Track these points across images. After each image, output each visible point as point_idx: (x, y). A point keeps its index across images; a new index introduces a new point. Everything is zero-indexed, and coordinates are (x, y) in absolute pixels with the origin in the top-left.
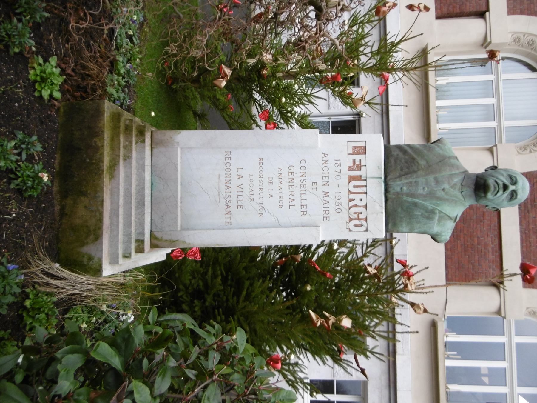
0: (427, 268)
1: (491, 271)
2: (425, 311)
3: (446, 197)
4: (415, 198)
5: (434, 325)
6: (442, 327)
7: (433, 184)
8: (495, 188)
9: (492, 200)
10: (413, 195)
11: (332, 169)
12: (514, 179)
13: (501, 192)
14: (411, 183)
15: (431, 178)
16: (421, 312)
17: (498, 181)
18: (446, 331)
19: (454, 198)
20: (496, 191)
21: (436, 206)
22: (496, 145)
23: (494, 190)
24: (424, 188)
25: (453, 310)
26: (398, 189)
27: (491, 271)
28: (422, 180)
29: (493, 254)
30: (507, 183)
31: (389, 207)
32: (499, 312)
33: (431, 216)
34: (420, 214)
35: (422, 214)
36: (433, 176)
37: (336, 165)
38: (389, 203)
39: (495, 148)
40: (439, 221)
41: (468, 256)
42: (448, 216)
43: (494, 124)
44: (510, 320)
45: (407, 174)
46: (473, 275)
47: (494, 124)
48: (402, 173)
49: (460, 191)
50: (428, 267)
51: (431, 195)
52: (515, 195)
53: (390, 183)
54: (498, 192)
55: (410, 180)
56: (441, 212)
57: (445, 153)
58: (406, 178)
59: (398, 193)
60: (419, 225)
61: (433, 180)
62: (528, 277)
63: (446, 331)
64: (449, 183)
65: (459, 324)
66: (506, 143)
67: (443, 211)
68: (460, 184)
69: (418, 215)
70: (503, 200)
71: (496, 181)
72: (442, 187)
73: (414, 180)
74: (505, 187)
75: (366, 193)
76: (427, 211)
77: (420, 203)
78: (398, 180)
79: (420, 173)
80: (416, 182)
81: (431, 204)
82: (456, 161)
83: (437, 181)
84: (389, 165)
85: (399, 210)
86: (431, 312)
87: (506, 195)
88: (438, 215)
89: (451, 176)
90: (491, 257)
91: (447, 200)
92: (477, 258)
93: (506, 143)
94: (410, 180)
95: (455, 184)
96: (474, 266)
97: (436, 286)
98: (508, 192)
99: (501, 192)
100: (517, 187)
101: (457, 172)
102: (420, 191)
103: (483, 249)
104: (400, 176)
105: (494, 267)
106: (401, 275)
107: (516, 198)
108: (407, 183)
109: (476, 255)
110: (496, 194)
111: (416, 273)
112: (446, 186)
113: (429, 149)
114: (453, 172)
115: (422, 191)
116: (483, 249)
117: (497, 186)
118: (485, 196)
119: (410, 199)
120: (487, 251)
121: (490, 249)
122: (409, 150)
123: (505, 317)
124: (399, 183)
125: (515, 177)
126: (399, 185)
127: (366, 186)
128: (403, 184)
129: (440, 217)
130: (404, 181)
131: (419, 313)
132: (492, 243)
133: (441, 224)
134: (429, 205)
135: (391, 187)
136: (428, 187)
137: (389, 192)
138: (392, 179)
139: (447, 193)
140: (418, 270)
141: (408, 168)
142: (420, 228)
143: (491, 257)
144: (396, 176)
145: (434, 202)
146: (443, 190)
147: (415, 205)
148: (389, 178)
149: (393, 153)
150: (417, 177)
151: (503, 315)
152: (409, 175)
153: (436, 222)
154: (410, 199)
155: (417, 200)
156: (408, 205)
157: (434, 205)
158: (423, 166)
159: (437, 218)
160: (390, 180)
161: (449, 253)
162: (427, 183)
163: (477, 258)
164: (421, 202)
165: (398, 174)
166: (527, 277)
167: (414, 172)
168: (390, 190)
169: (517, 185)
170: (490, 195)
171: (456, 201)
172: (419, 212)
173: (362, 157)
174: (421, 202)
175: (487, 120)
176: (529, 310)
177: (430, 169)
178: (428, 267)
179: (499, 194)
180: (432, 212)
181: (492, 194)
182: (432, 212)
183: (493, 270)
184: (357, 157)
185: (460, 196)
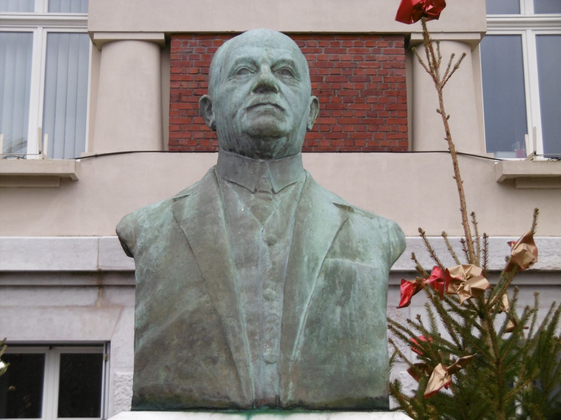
0: (423, 234)
1: (380, 57)
2: (528, 239)
3: (289, 236)
4: (297, 324)
5: (511, 183)
6: (513, 164)
7: (255, 272)
8: (266, 113)
9: (296, 117)
10: (289, 330)
12: (242, 65)
13: (277, 98)
14: (252, 334)
15: (238, 277)
16: (532, 248)
17: (248, 104)
18: (522, 154)
19: (293, 213)
20: (276, 110)
21: (316, 264)
22: (91, 34)
23: (273, 114)
24: (267, 298)
25: (471, 134)
26: (270, 371)
27: (380, 57)
28: (244, 304)
29: (343, 52)
30: (252, 82)
31: (321, 400)
32: (471, 45)
33: (343, 279)
34: (338, 310)
35: (339, 303)
36: (233, 270)
38: (309, 398)
39: (97, 37)
40: (354, 255)
41: (346, 102)
42: (341, 229)
43: (39, 36)
44: (489, 22)
45: (225, 345)
46: (391, 94)
47: (39, 36)
48: (223, 357)
49: (271, 196)
50: (420, 230)
51: (289, 277)
52: (283, 65)
53: (250, 397)
54: (276, 106)
55: (245, 337)
56: (331, 252)
57: (166, 229)
58: (238, 349)
59: (282, 374)
60: (369, 312)
61: (243, 270)
62: (431, 7)
63: (522, 154)
64: (252, 227)
65: (504, 130)
66: (87, 11)
67: (329, 244)
68: (253, 197)
69: (343, 315)
70: (295, 92)
71: (249, 109)
72: (265, 246)
73: (245, 325)
74: (265, 88)
76: (328, 290)
77: (310, 309)
78: (242, 373)
79: (223, 306)
80: (249, 321)
81: (310, 280)
82: (187, 202)
83: (248, 260)
84: (196, 395)
85: (330, 369)
86: (531, 226)
87: (283, 87)
88: (339, 260)
89: (234, 221)
90: (348, 56)
91: (298, 235)
92: (351, 85)
93: (87, 11)
94: (245, 337)
95: (254, 209)
96: (369, 92)
97: (463, 210)
98: (278, 82)
99: (277, 98)
100: (264, 61)
101: (219, 203)
102: (276, 308)
103: (330, 71)
104: (231, 363)
105: (370, 49)
106: (443, 298)
107: (292, 63)
108: (253, 346)
109: (344, 85)
110: (282, 110)
111: (436, 260)
112: (260, 236)
113: (154, 277)
114: (221, 214)
115: (275, 303)
116: (330, 71)
117: (261, 108)
118: (287, 135)
119: (300, 339)
120: (335, 63)
121: (331, 56)
122: (150, 335)
123: (483, 34)
124: (252, 369)
125: (237, 63)
126: (258, 369)
128: (256, 357)
129: (344, 254)
130: (247, 352)
131: (536, 253)
132: (317, 51)
133: (361, 249)
134: (313, 286)
135: (264, 393)
136: (265, 287)
137: (278, 398)
138: (239, 388)
139: (280, 235)
140: (428, 254)
141: (207, 343)
142: (375, 308)
143: (348, 56)
144: (233, 376)
145: (304, 269)
146: (270, 243)
147: (314, 323)
148: (237, 399)
149: (161, 381)
150: (236, 315)
151: (478, 37)
152: (230, 337)
153: (358, 262)
154: (300, 339)
155: (303, 319)
156: (315, 345)
157: (314, 270)
158: (205, 298)
159: (347, 262)
160: (243, 397)
161: (341, 142)
162: (253, 289)
163: (351, 85)
164: (306, 306)
165: (226, 372)
166: (430, 11)
167: (220, 324)
168: (271, 395)
169: (260, 60)
170: (285, 126)
171: (300, 208)
172: (333, 312)
174: (306, 306)
175: (27, 47)
177: (212, 277)
178: (420, 230)
179: (283, 104)
180: (332, 274)
181: (282, 120)
182: (332, 274)
183: (378, 51)
185: (287, 195)
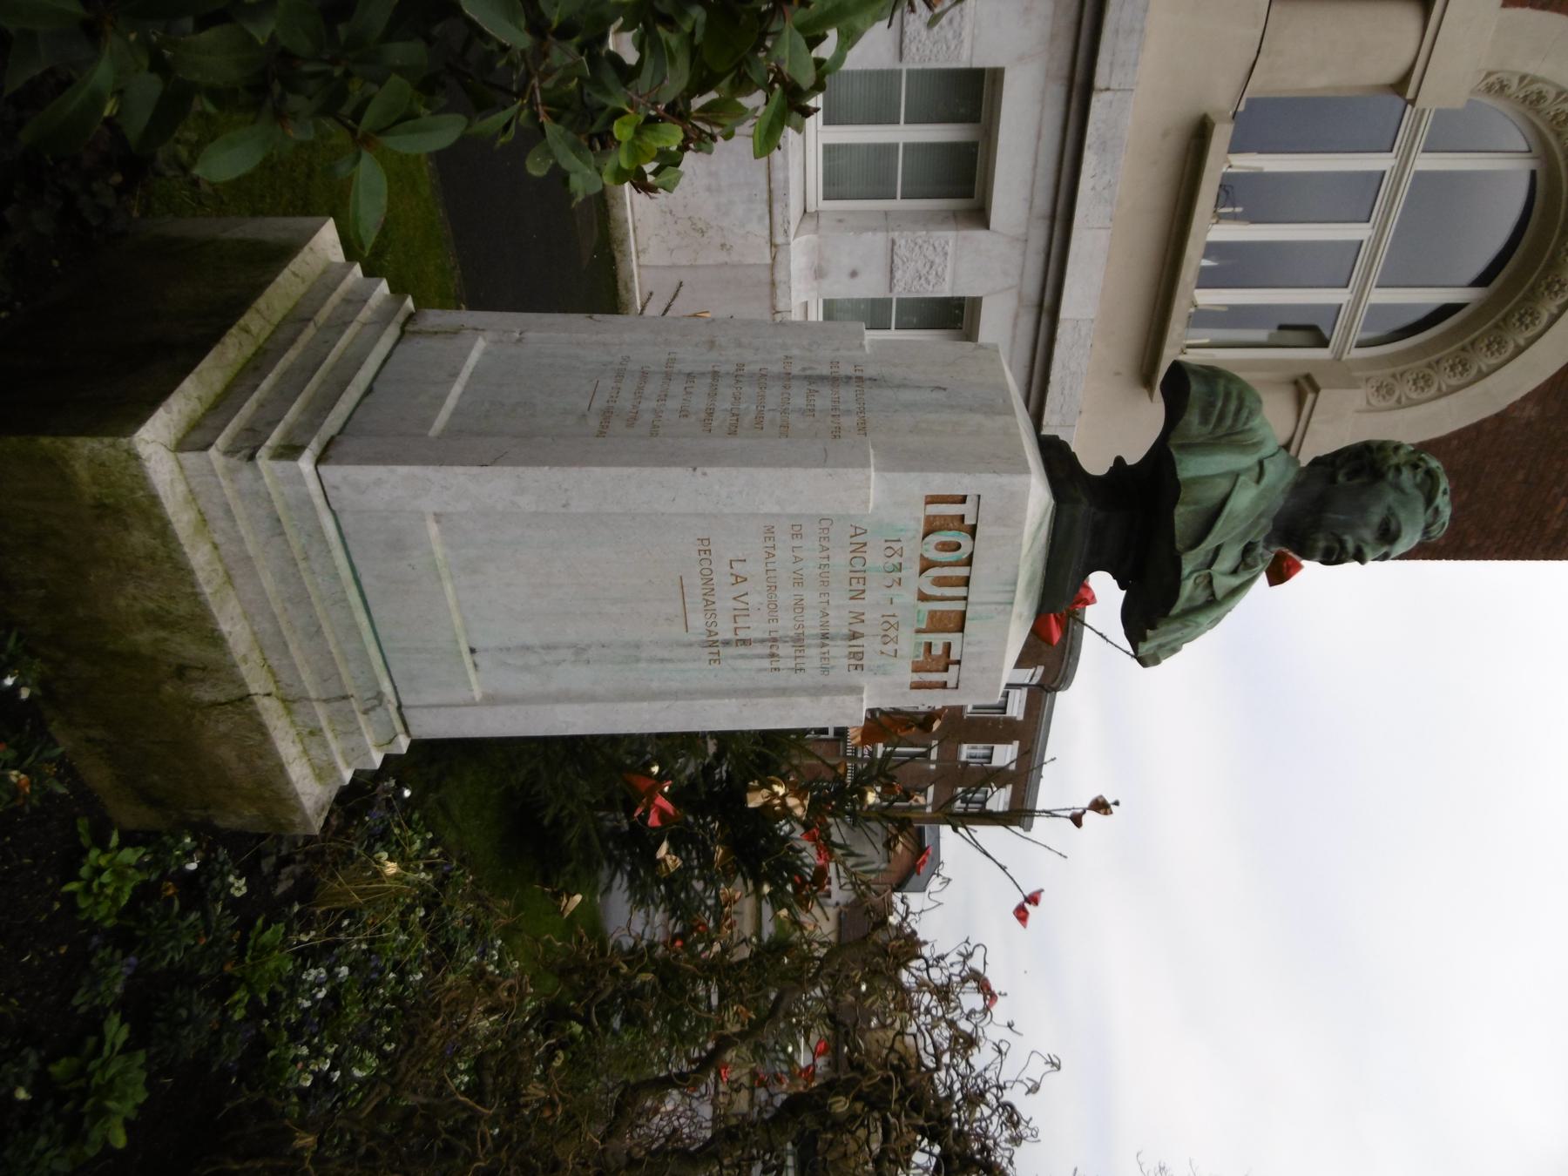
11: (875, 558)
32: (1400, 86)
37: (889, 552)
75: (965, 598)
123: (1413, 102)
127: (966, 582)
173: (954, 638)
176: (1492, 79)
184: (938, 640)
